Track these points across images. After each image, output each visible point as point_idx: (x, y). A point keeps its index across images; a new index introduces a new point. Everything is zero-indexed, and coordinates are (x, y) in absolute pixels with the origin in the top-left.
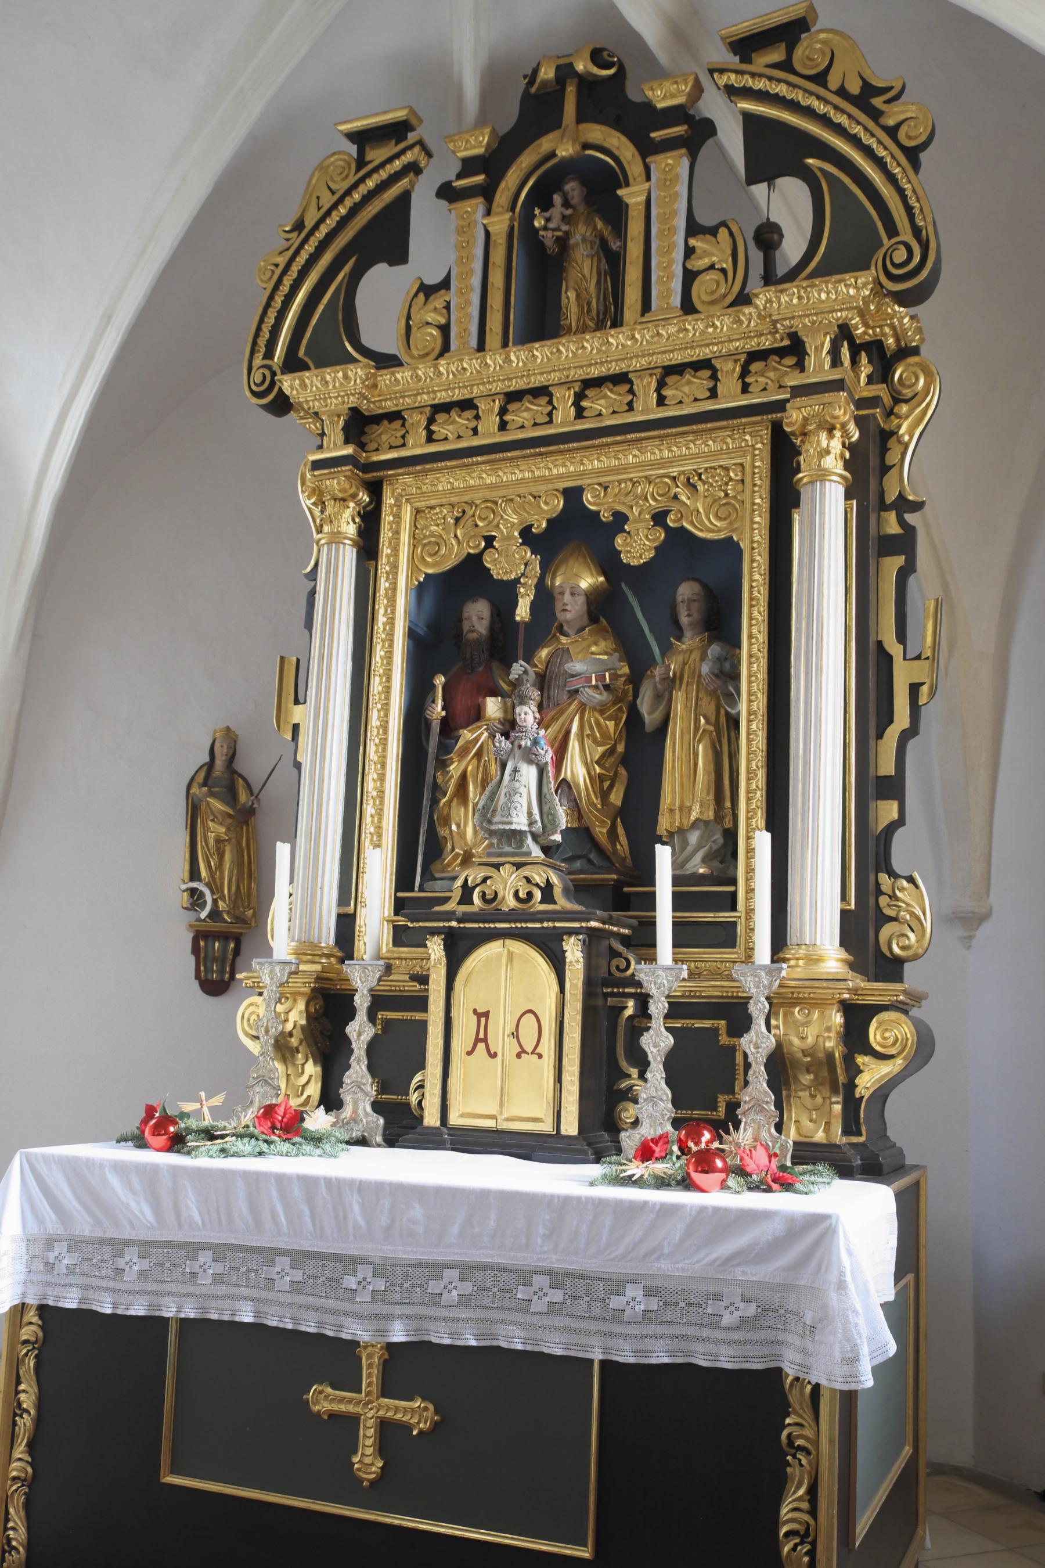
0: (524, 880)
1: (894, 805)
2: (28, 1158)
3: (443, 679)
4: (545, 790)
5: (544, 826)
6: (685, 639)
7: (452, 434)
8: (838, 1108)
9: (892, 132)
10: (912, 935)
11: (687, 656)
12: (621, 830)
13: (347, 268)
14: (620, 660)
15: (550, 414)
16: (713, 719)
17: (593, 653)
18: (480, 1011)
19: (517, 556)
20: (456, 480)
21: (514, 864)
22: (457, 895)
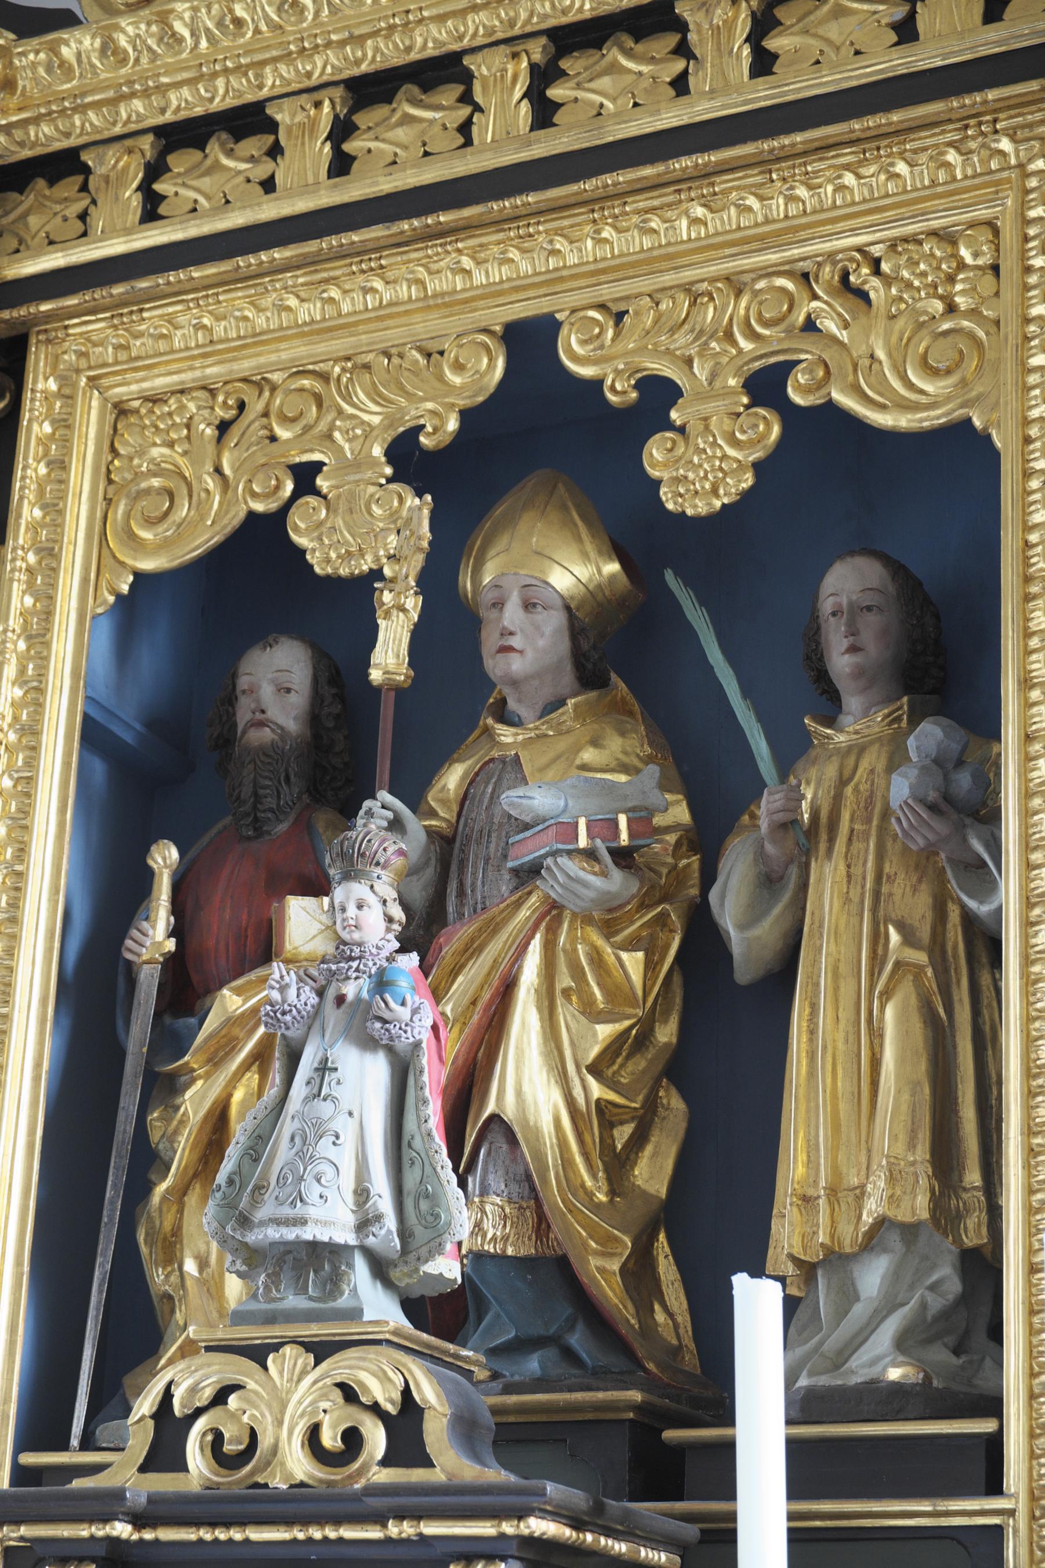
0: (337, 1395)
3: (174, 854)
4: (410, 1123)
5: (404, 1233)
6: (845, 719)
7: (208, 198)
11: (851, 761)
12: (667, 1269)
14: (664, 786)
15: (465, 128)
16: (925, 933)
17: (584, 767)
19: (377, 510)
20: (218, 318)
21: (308, 1346)
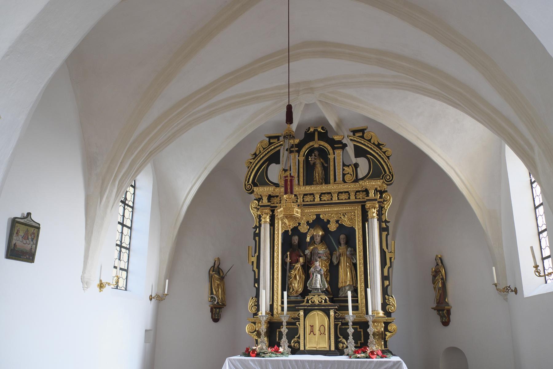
1: (388, 282)
2: (230, 359)
8: (383, 343)
9: (384, 153)
10: (392, 307)
13: (266, 164)
15: (314, 199)
18: (311, 325)
21: (318, 295)
22: (305, 301)
